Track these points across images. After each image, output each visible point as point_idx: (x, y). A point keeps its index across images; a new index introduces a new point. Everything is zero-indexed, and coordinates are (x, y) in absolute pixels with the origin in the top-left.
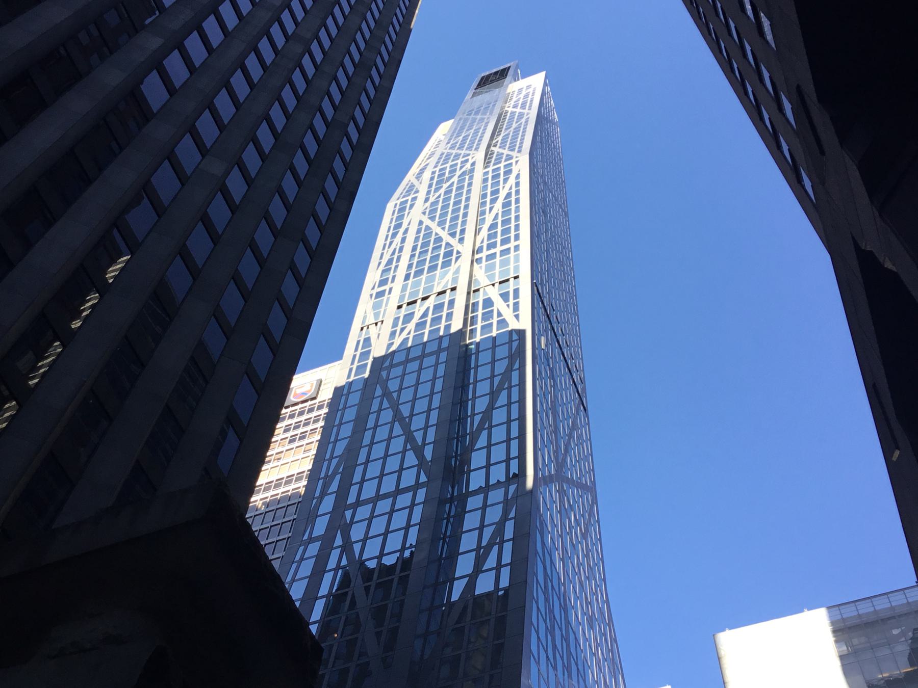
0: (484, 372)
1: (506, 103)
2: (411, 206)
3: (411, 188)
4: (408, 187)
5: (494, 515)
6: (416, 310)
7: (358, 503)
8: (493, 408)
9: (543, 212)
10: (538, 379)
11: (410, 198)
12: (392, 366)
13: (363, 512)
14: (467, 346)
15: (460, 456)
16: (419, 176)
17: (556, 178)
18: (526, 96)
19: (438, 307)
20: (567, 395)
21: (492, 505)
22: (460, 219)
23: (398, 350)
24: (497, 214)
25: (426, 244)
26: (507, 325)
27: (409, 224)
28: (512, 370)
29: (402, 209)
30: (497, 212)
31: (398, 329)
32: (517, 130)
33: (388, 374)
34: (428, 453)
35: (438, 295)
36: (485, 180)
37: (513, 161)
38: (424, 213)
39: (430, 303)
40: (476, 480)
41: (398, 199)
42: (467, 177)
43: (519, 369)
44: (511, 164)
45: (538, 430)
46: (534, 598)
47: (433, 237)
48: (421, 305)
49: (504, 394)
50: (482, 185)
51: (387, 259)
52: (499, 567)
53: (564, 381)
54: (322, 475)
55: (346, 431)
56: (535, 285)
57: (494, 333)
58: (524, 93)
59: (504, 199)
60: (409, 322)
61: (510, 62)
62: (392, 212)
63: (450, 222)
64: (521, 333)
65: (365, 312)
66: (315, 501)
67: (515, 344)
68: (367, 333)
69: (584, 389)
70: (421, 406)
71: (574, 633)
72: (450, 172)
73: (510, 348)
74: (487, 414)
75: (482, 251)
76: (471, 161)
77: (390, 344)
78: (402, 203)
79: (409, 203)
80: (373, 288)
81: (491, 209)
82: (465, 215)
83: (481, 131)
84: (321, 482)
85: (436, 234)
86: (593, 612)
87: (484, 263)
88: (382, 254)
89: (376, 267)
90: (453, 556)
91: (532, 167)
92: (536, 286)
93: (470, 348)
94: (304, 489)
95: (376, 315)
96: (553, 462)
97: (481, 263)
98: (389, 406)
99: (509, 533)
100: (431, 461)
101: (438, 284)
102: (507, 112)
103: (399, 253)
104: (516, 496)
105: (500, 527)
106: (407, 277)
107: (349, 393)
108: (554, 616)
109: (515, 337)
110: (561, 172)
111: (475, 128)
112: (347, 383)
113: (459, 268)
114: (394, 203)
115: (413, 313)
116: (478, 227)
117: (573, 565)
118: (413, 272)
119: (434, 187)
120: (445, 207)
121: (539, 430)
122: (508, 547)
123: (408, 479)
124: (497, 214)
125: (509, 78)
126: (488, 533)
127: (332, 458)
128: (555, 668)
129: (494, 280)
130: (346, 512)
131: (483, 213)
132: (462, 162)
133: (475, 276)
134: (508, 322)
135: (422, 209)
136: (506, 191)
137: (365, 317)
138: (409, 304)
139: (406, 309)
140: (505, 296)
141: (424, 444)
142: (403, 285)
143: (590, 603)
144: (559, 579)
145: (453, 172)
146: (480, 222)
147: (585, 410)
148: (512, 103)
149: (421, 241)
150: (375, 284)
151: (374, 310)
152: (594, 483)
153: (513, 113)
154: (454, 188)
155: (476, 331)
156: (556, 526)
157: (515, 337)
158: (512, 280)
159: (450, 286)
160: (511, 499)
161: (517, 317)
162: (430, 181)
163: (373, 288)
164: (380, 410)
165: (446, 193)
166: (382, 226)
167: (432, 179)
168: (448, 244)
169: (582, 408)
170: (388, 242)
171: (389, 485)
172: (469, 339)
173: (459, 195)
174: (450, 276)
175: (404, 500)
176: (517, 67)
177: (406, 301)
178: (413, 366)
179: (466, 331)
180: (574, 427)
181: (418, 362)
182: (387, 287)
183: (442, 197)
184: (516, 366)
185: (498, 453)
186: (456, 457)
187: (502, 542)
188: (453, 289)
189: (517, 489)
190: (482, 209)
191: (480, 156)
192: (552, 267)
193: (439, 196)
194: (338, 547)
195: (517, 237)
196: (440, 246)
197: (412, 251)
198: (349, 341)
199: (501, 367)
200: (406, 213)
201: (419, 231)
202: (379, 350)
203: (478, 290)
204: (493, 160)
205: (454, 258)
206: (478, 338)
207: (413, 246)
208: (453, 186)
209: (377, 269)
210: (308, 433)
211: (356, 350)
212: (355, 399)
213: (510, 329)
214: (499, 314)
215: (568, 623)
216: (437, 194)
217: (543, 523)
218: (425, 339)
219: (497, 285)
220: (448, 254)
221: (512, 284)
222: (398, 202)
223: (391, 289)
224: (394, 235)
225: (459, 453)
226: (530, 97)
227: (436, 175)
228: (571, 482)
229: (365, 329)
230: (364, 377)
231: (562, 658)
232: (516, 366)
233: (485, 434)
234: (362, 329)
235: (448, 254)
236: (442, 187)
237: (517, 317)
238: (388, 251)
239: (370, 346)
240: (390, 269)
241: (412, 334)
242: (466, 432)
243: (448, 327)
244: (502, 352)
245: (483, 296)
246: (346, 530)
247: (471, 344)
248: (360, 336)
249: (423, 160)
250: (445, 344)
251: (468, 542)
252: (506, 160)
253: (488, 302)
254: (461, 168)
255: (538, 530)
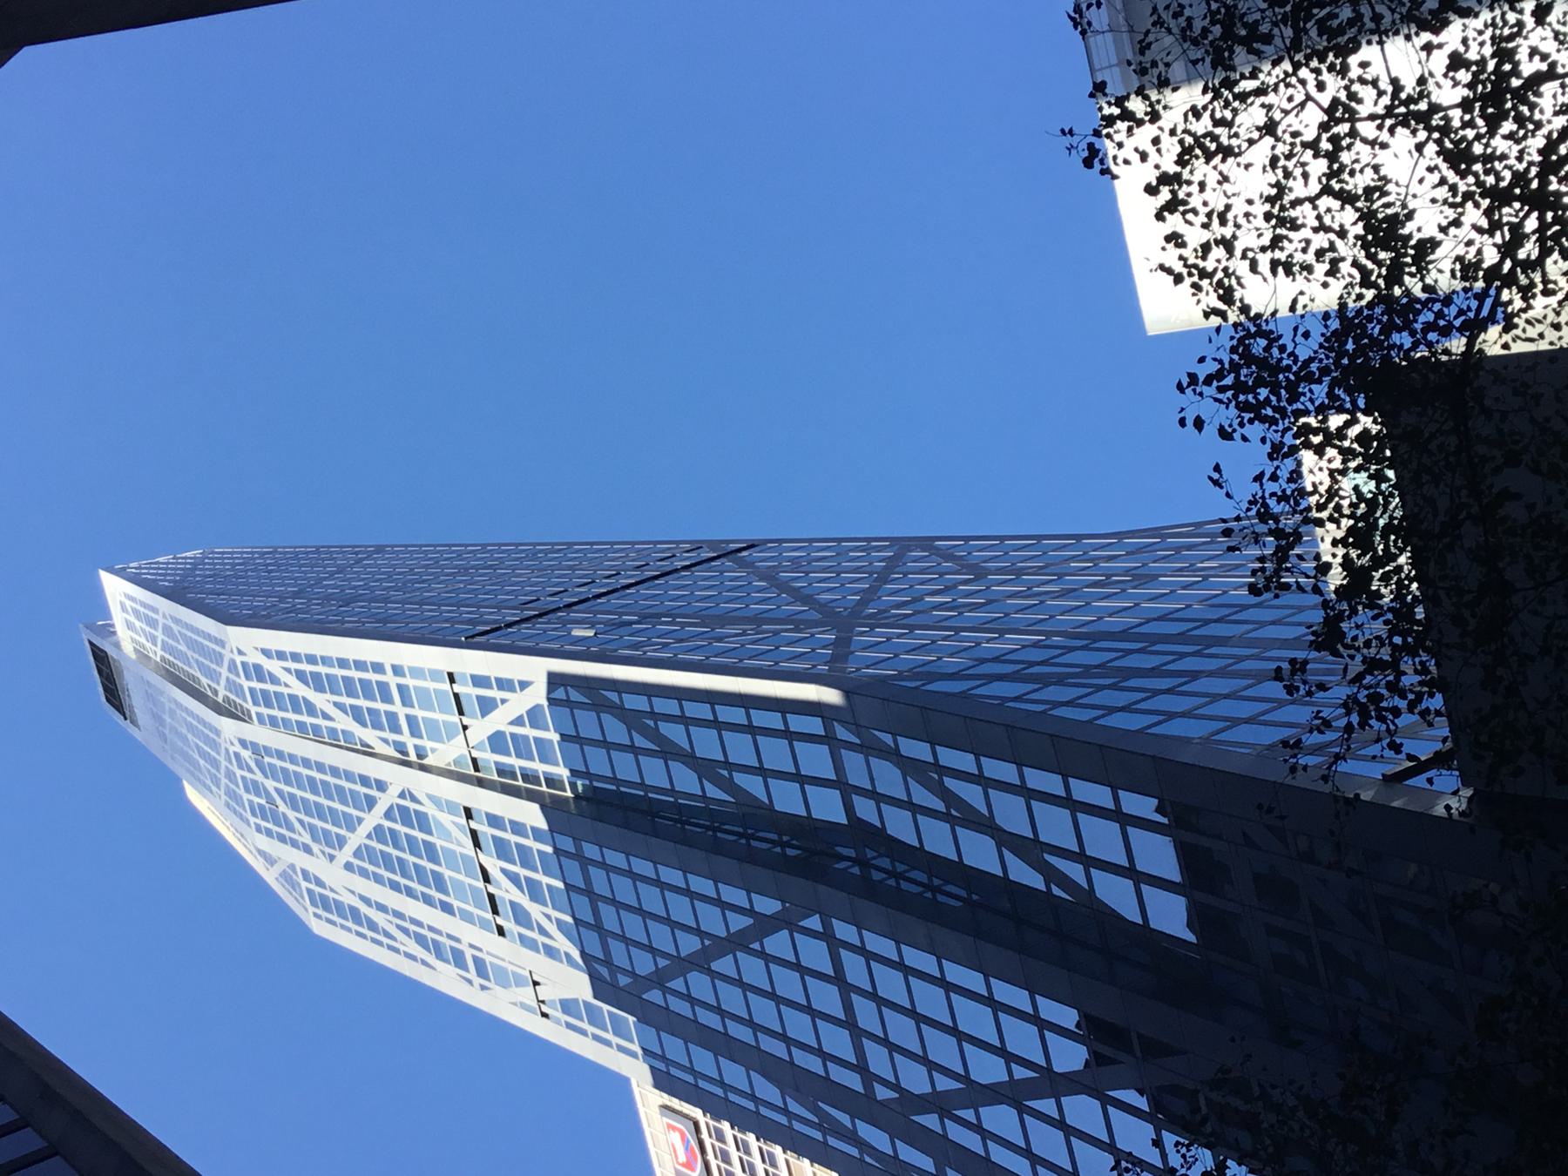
0: (625, 767)
1: (150, 658)
2: (319, 883)
3: (287, 877)
4: (287, 886)
5: (889, 779)
6: (507, 897)
7: (861, 1068)
8: (692, 755)
9: (347, 605)
10: (645, 653)
11: (304, 884)
12: (608, 962)
13: (878, 1059)
14: (577, 797)
15: (714, 822)
16: (270, 860)
17: (426, 566)
18: (136, 613)
19: (502, 849)
20: (702, 588)
21: (872, 780)
22: (343, 783)
23: (579, 944)
24: (336, 704)
25: (387, 861)
26: (538, 707)
27: (353, 892)
28: (622, 708)
29: (325, 903)
30: (332, 705)
31: (541, 939)
32: (192, 644)
33: (625, 972)
34: (768, 905)
35: (480, 849)
36: (273, 722)
37: (239, 659)
38: (332, 858)
39: (493, 865)
40: (827, 806)
41: (306, 910)
42: (267, 759)
43: (620, 693)
44: (244, 664)
45: (740, 665)
46: (1044, 712)
47: (374, 844)
48: (499, 887)
49: (667, 729)
50: (282, 730)
51: (416, 945)
52: (979, 779)
53: (673, 593)
54: (818, 1135)
55: (735, 1074)
56: (470, 640)
57: (554, 737)
58: (132, 619)
59: (308, 686)
60: (527, 915)
61: (82, 640)
62: (358, 938)
63: (413, 828)
64: (555, 680)
65: (515, 1004)
66: (868, 1159)
67: (575, 696)
68: (552, 1004)
69: (712, 544)
70: (680, 909)
71: (1148, 621)
72: (258, 794)
73: (581, 705)
74: (704, 768)
75: (404, 745)
76: (238, 748)
77: (521, 942)
78: (314, 903)
79: (312, 887)
80: (470, 982)
81: (326, 716)
82: (335, 772)
83: (189, 719)
84: (832, 1141)
85: (369, 836)
86: (1127, 572)
87: (428, 744)
88: (408, 955)
89: (431, 970)
90: (958, 871)
91: (253, 620)
92: (473, 637)
93: (583, 790)
94: (816, 1165)
95: (519, 982)
96: (812, 635)
97: (424, 748)
98: (682, 978)
99: (916, 749)
100: (783, 902)
101: (459, 844)
102: (163, 659)
103: (405, 920)
104: (856, 727)
105: (910, 767)
106: (447, 908)
107: (663, 1058)
108: (1096, 667)
109: (560, 694)
110: (297, 554)
111: (184, 731)
112: (644, 1061)
113: (431, 797)
114: (312, 918)
115: (512, 903)
116: (359, 747)
117: (1069, 611)
118: (438, 896)
119: (283, 831)
120: (320, 812)
121: (707, 658)
122: (949, 757)
123: (815, 954)
124: (336, 704)
125: (111, 652)
126: (922, 796)
127: (785, 1111)
128: (1194, 675)
129: (456, 724)
130: (879, 1098)
131: (333, 732)
132: (241, 767)
133: (449, 764)
134: (532, 705)
135: (324, 861)
136: (292, 680)
137: (524, 1006)
138: (495, 911)
139: (504, 919)
140: (487, 706)
141: (750, 912)
142: (462, 919)
143: (1108, 576)
144: (1036, 645)
145: (256, 788)
146: (336, 740)
147: (752, 546)
148: (148, 645)
149: (381, 871)
150: (461, 976)
151: (511, 986)
152: (893, 540)
153: (165, 647)
154: (287, 789)
155: (503, 764)
156: (933, 642)
157: (560, 694)
158: (457, 689)
159: (463, 821)
160: (859, 738)
161: (524, 685)
162: (272, 837)
163: (470, 982)
164: (688, 998)
165: (295, 808)
166: (371, 956)
167: (269, 833)
168: (388, 815)
169: (744, 554)
170: (386, 941)
171: (827, 998)
172: (565, 791)
173: (298, 781)
174: (446, 819)
175: (855, 968)
176: (91, 627)
177: (489, 916)
178: (608, 915)
179: (551, 795)
180: (770, 576)
181: (856, 999)
182: (469, 953)
183: (302, 816)
184: (613, 696)
185: (776, 754)
186: (784, 845)
187: (936, 765)
188: (469, 813)
189: (842, 722)
190: (326, 735)
191: (227, 726)
192: (516, 597)
193: (301, 822)
194: (943, 1124)
195: (378, 668)
196: (391, 831)
197: (400, 891)
198: (567, 1047)
199: (617, 731)
200: (331, 895)
201: (364, 873)
202: (579, 986)
203: (474, 761)
204: (238, 701)
205: (412, 806)
206: (563, 772)
207: (391, 888)
208: (282, 790)
209: (434, 969)
210: (745, 1157)
211: (583, 1033)
212: (675, 1047)
213: (545, 703)
214: (518, 721)
215: (1125, 634)
216: (297, 825)
217: (918, 673)
218: (560, 885)
219: (466, 721)
220: (405, 816)
221: (466, 690)
222: (311, 909)
223: (471, 946)
224: (372, 926)
225: (741, 830)
226: (138, 607)
227: (263, 824)
228: (869, 596)
229: (545, 1009)
230: (634, 1022)
231: (1182, 655)
232: (613, 696)
233: (741, 779)
234: (544, 1015)
235: (405, 816)
236: (284, 814)
237: (524, 685)
238: (401, 943)
239: (576, 1001)
240: (435, 942)
241: (549, 911)
242: (641, 796)
243: (537, 834)
244: (588, 724)
245: (485, 751)
246: (911, 1102)
247: (573, 786)
248: (558, 1022)
249: (245, 846)
250: (567, 844)
251: (938, 839)
252: (238, 675)
253: (497, 742)
254: (250, 770)
255: (923, 685)
